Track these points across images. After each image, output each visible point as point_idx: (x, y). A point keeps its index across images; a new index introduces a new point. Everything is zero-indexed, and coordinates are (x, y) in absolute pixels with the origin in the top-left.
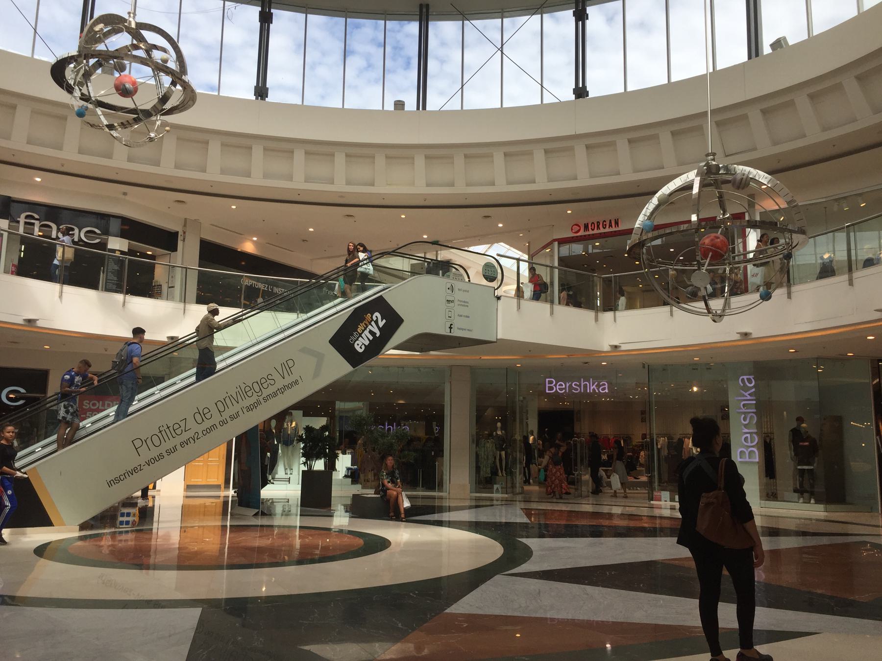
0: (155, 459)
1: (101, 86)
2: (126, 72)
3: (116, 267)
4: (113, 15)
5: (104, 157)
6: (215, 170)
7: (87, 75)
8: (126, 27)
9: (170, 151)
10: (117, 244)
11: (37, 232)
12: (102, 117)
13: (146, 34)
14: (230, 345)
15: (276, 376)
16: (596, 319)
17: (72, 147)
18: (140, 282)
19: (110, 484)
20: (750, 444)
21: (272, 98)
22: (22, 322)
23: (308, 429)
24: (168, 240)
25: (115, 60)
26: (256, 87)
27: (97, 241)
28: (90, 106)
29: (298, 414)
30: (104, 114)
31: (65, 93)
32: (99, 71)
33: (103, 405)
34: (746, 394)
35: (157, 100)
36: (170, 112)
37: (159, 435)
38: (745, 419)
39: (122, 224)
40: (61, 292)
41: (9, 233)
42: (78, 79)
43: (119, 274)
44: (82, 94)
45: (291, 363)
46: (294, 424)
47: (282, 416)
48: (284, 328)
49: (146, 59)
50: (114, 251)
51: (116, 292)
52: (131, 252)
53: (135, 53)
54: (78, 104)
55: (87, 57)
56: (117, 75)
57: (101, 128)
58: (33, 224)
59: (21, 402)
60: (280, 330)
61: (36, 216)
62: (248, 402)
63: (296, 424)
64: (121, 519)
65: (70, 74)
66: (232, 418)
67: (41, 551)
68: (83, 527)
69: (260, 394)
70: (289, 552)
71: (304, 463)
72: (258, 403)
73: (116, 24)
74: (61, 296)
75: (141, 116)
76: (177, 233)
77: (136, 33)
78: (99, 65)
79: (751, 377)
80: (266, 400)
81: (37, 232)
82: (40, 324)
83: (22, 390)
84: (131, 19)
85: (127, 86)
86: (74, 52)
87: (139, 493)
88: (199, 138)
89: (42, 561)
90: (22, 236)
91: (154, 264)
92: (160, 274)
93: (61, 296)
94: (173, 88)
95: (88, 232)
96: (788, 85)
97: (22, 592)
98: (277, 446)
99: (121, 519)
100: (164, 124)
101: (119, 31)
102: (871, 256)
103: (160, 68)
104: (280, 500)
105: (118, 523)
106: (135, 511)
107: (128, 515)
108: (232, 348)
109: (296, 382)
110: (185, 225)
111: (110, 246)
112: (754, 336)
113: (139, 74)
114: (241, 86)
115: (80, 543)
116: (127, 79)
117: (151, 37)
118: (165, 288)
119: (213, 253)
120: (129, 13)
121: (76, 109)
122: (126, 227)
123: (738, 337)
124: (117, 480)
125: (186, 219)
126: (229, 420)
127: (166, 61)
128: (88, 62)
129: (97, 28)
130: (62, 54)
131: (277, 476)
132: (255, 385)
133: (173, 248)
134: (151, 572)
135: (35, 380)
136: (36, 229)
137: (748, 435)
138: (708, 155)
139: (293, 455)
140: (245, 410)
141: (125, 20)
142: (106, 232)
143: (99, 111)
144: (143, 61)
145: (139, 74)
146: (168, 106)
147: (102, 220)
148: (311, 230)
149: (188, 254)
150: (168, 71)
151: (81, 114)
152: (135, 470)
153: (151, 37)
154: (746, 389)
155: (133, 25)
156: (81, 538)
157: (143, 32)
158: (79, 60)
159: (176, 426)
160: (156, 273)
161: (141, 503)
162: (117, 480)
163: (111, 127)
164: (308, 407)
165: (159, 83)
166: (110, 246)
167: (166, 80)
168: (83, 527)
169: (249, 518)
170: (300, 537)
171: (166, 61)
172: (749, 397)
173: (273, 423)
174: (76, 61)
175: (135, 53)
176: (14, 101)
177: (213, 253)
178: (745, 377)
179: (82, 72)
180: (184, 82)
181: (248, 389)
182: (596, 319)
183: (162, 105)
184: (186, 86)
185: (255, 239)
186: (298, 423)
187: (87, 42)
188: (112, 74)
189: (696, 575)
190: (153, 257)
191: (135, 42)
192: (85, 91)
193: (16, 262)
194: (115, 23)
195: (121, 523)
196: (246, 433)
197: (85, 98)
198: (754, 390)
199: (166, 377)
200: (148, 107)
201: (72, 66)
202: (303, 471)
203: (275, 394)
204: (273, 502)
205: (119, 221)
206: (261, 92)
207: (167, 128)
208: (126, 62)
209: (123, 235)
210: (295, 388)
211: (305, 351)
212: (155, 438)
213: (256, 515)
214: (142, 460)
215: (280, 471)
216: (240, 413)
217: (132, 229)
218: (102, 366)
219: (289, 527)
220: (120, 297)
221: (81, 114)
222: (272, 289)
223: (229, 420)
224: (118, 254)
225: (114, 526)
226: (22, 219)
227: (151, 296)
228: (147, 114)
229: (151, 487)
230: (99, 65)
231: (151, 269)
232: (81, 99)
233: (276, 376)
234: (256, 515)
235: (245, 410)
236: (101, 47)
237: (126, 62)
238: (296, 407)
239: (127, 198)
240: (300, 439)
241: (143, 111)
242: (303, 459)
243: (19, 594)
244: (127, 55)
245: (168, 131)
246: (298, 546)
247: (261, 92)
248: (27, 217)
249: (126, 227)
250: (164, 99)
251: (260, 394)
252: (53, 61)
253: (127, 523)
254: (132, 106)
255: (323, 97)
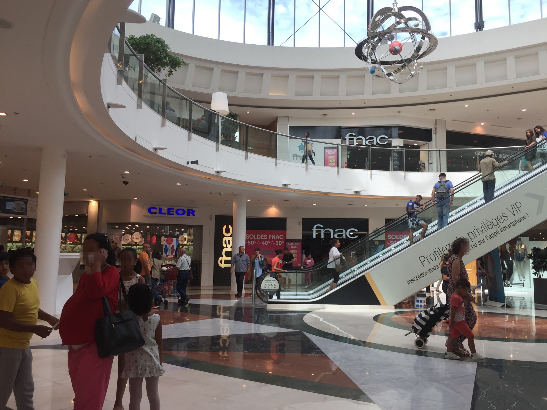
0: (433, 269)
1: (382, 53)
2: (394, 40)
3: (398, 156)
4: (383, 9)
5: (386, 93)
6: (453, 85)
7: (374, 49)
8: (393, 13)
9: (423, 80)
10: (397, 142)
11: (355, 143)
12: (384, 70)
13: (404, 13)
14: (473, 196)
15: (509, 214)
16: (246, 157)
17: (370, 91)
18: (413, 164)
19: (409, 283)
21: (487, 27)
22: (353, 193)
23: (536, 250)
24: (426, 135)
25: (389, 34)
26: (475, 24)
27: (386, 142)
28: (377, 66)
29: (526, 239)
30: (385, 68)
31: (363, 62)
32: (380, 44)
33: (398, 237)
35: (413, 52)
36: (425, 54)
37: (434, 254)
39: (399, 130)
40: (371, 174)
41: (342, 146)
42: (369, 52)
43: (400, 160)
44: (372, 60)
45: (518, 205)
46: (523, 246)
47: (513, 242)
48: (511, 181)
49: (405, 28)
50: (396, 147)
51: (399, 170)
52: (405, 146)
53: (398, 27)
54: (368, 65)
55: (373, 38)
56: (389, 43)
57: (384, 77)
58: (353, 139)
59: (356, 237)
60: (508, 182)
61: (354, 134)
62: (490, 232)
63: (525, 246)
64: (417, 303)
65: (365, 51)
66: (480, 243)
67: (376, 318)
68: (396, 307)
69: (498, 226)
70: (528, 332)
71: (535, 273)
72: (497, 233)
73: (387, 13)
74: (371, 177)
75: (406, 63)
76: (431, 130)
77: (399, 15)
78: (380, 40)
80: (502, 230)
81: (355, 143)
82: (362, 193)
83: (356, 230)
84: (395, 7)
85: (396, 48)
86: (366, 37)
87: (425, 289)
88: (441, 66)
89: (377, 324)
90: (348, 147)
91: (419, 151)
92: (423, 156)
93: (371, 177)
94: (423, 41)
95: (381, 138)
97: (370, 340)
98: (512, 261)
99: (417, 303)
100: (419, 65)
101: (387, 17)
103: (415, 30)
104: (518, 298)
105: (416, 306)
106: (424, 299)
107: (421, 301)
108: (475, 198)
109: (524, 218)
110: (436, 124)
111: (393, 144)
113: (403, 38)
114: (465, 24)
115: (396, 316)
116: (396, 44)
117: (407, 14)
118: (427, 165)
119: (455, 138)
120: (393, 4)
121: (370, 69)
122: (401, 132)
124: (413, 281)
125: (436, 120)
126: (478, 244)
127: (417, 25)
128: (374, 40)
129: (377, 19)
130: (359, 40)
131: (514, 282)
132: (494, 221)
133: (430, 139)
134: (436, 336)
135: (363, 224)
136: (355, 141)
139: (524, 267)
140: (488, 238)
141: (391, 9)
142: (391, 137)
143: (382, 67)
144: (403, 30)
145: (403, 38)
146: (421, 52)
147: (387, 130)
148: (524, 110)
149: (439, 141)
150: (418, 31)
151: (372, 72)
152: (422, 275)
153: (407, 14)
155: (396, 11)
156: (396, 313)
157: (401, 12)
158: (369, 41)
159: (444, 249)
160: (420, 156)
161: (427, 295)
162: (413, 281)
163: (389, 74)
164: (533, 234)
165: (415, 41)
166: (393, 144)
167: (418, 37)
168: (396, 307)
169: (497, 308)
170: (536, 323)
171: (417, 25)
173: (508, 246)
174: (367, 42)
175: (398, 27)
176: (336, 74)
177: (455, 138)
179: (371, 47)
180: (429, 34)
181: (489, 224)
182: (246, 157)
183: (418, 53)
184: (431, 37)
185: (482, 124)
186: (527, 246)
187: (372, 29)
188: (386, 43)
189: (155, 329)
190: (418, 147)
191: (398, 20)
192: (373, 58)
193: (346, 161)
194: (386, 12)
195: (418, 306)
196: (489, 254)
197: (374, 62)
199: (433, 220)
200: (409, 57)
201: (365, 45)
202: (534, 279)
203: (509, 227)
204: (512, 299)
205: (397, 129)
206: (479, 25)
207: (421, 66)
208: (394, 34)
209: (400, 136)
210: (524, 221)
211: (529, 195)
212: (432, 256)
213: (503, 307)
214: (426, 269)
215: (516, 278)
216: (485, 239)
217: (406, 132)
218: (400, 213)
219: (526, 316)
220: (402, 173)
221: (372, 72)
222: (498, 156)
223: (478, 244)
224: (398, 148)
225: (414, 308)
226: (347, 137)
227: (419, 170)
228: (409, 61)
229: (431, 286)
230: (380, 40)
231: (418, 154)
232: (372, 63)
233: (509, 214)
234: (503, 307)
235: (488, 238)
236: (380, 30)
237: (394, 34)
238: (524, 235)
239: (400, 114)
240: (530, 257)
241: (406, 60)
242: (534, 271)
243: (368, 340)
244: (394, 29)
245: (422, 68)
246: (534, 329)
247: (479, 25)
248: (350, 136)
249: (401, 132)
250: (419, 49)
251: (498, 226)
252: (355, 45)
253: (421, 306)
254: (400, 59)
255: (522, 16)
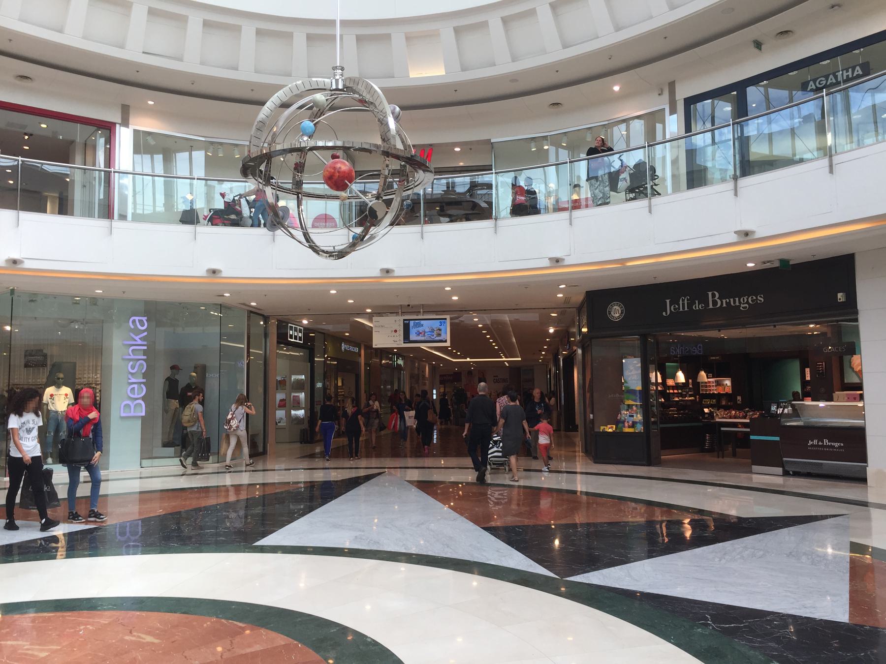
20: (136, 396)
34: (137, 338)
38: (133, 367)
64: (300, 335)
79: (144, 319)
96: (100, 81)
99: (300, 335)
102: (537, 191)
112: (224, 275)
123: (734, 238)
137: (135, 386)
138: (335, 68)
154: (137, 332)
172: (140, 342)
178: (137, 318)
198: (145, 334)
